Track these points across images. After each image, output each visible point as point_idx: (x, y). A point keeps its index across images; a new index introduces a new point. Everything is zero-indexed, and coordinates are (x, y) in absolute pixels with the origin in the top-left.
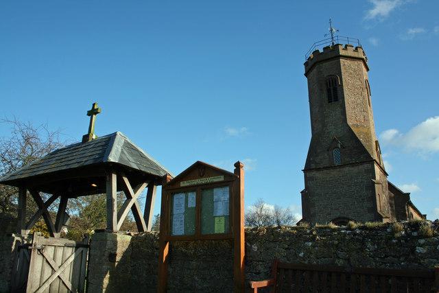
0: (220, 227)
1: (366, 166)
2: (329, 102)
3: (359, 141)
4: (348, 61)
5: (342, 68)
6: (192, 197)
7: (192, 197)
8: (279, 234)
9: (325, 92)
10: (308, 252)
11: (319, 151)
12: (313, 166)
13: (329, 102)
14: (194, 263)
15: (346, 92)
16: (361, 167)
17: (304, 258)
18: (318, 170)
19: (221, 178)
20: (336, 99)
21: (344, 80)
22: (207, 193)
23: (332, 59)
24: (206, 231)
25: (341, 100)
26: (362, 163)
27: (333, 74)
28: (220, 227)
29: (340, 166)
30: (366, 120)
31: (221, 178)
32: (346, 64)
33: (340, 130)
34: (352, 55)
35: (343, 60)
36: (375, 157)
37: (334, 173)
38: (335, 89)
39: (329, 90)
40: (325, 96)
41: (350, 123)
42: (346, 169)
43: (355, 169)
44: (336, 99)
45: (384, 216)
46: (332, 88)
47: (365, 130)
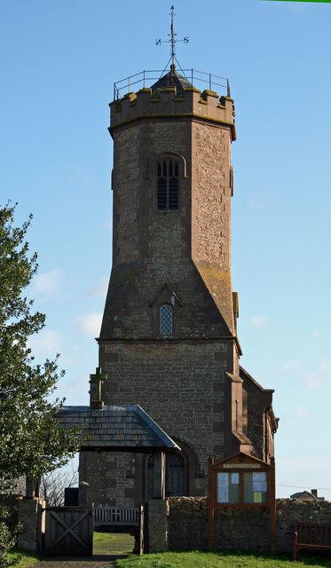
0: (258, 499)
1: (218, 347)
2: (160, 207)
3: (210, 297)
4: (206, 128)
5: (194, 141)
6: (235, 478)
7: (235, 478)
8: (295, 504)
9: (154, 183)
10: (315, 516)
11: (132, 304)
12: (118, 333)
13: (160, 207)
14: (232, 522)
15: (196, 194)
16: (209, 347)
17: (312, 520)
18: (130, 341)
19: (259, 466)
20: (174, 205)
21: (193, 170)
22: (246, 475)
23: (177, 118)
24: (247, 500)
25: (184, 209)
26: (212, 340)
27: (175, 151)
28: (258, 499)
29: (170, 341)
30: (224, 254)
31: (259, 466)
32: (201, 133)
33: (175, 270)
34: (214, 118)
35: (197, 125)
36: (234, 335)
37: (158, 352)
38: (174, 183)
39: (161, 183)
40: (152, 192)
41: (195, 259)
42: (182, 347)
43: (199, 350)
44: (174, 205)
45: (242, 441)
46: (168, 178)
47: (219, 275)
